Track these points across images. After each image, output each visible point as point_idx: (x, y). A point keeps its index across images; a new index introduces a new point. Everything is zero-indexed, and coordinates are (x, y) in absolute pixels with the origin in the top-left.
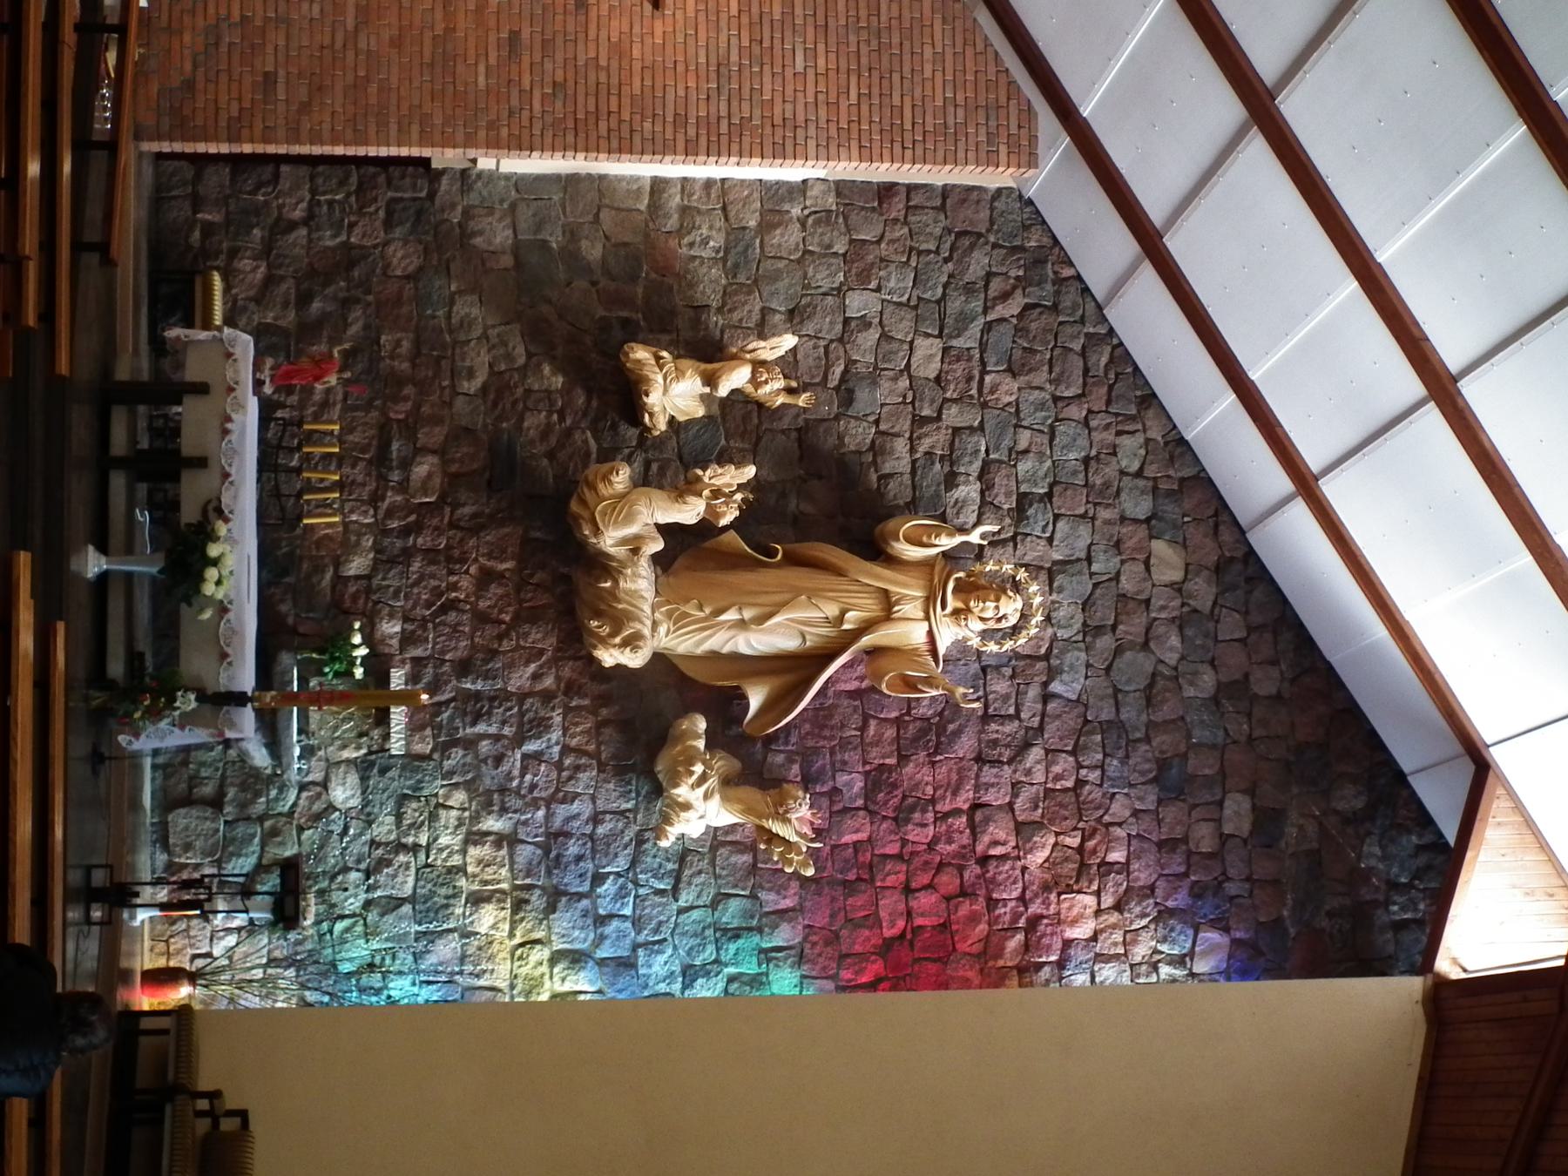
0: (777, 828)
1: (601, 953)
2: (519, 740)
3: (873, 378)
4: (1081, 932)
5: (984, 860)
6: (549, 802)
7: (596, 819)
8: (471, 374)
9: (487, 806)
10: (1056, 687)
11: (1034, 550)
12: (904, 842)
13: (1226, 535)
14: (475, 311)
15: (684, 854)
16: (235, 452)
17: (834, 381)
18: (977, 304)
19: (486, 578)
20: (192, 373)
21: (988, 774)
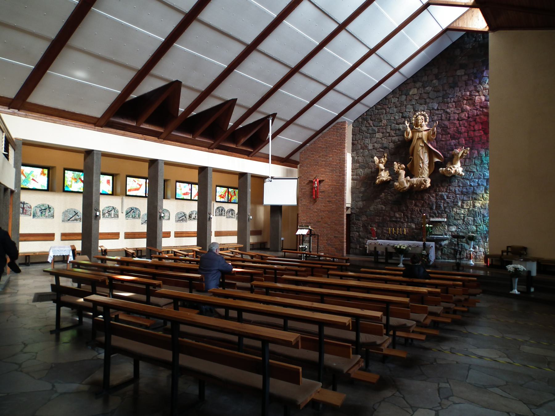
0: (460, 155)
1: (485, 184)
2: (444, 199)
3: (382, 144)
4: (483, 98)
5: (468, 117)
6: (456, 194)
7: (459, 186)
8: (382, 208)
9: (456, 205)
10: (436, 108)
11: (411, 114)
12: (465, 132)
13: (409, 81)
14: (372, 207)
15: (466, 171)
16: (385, 243)
17: (383, 150)
18: (370, 128)
19: (416, 205)
20: (373, 249)
21: (452, 118)
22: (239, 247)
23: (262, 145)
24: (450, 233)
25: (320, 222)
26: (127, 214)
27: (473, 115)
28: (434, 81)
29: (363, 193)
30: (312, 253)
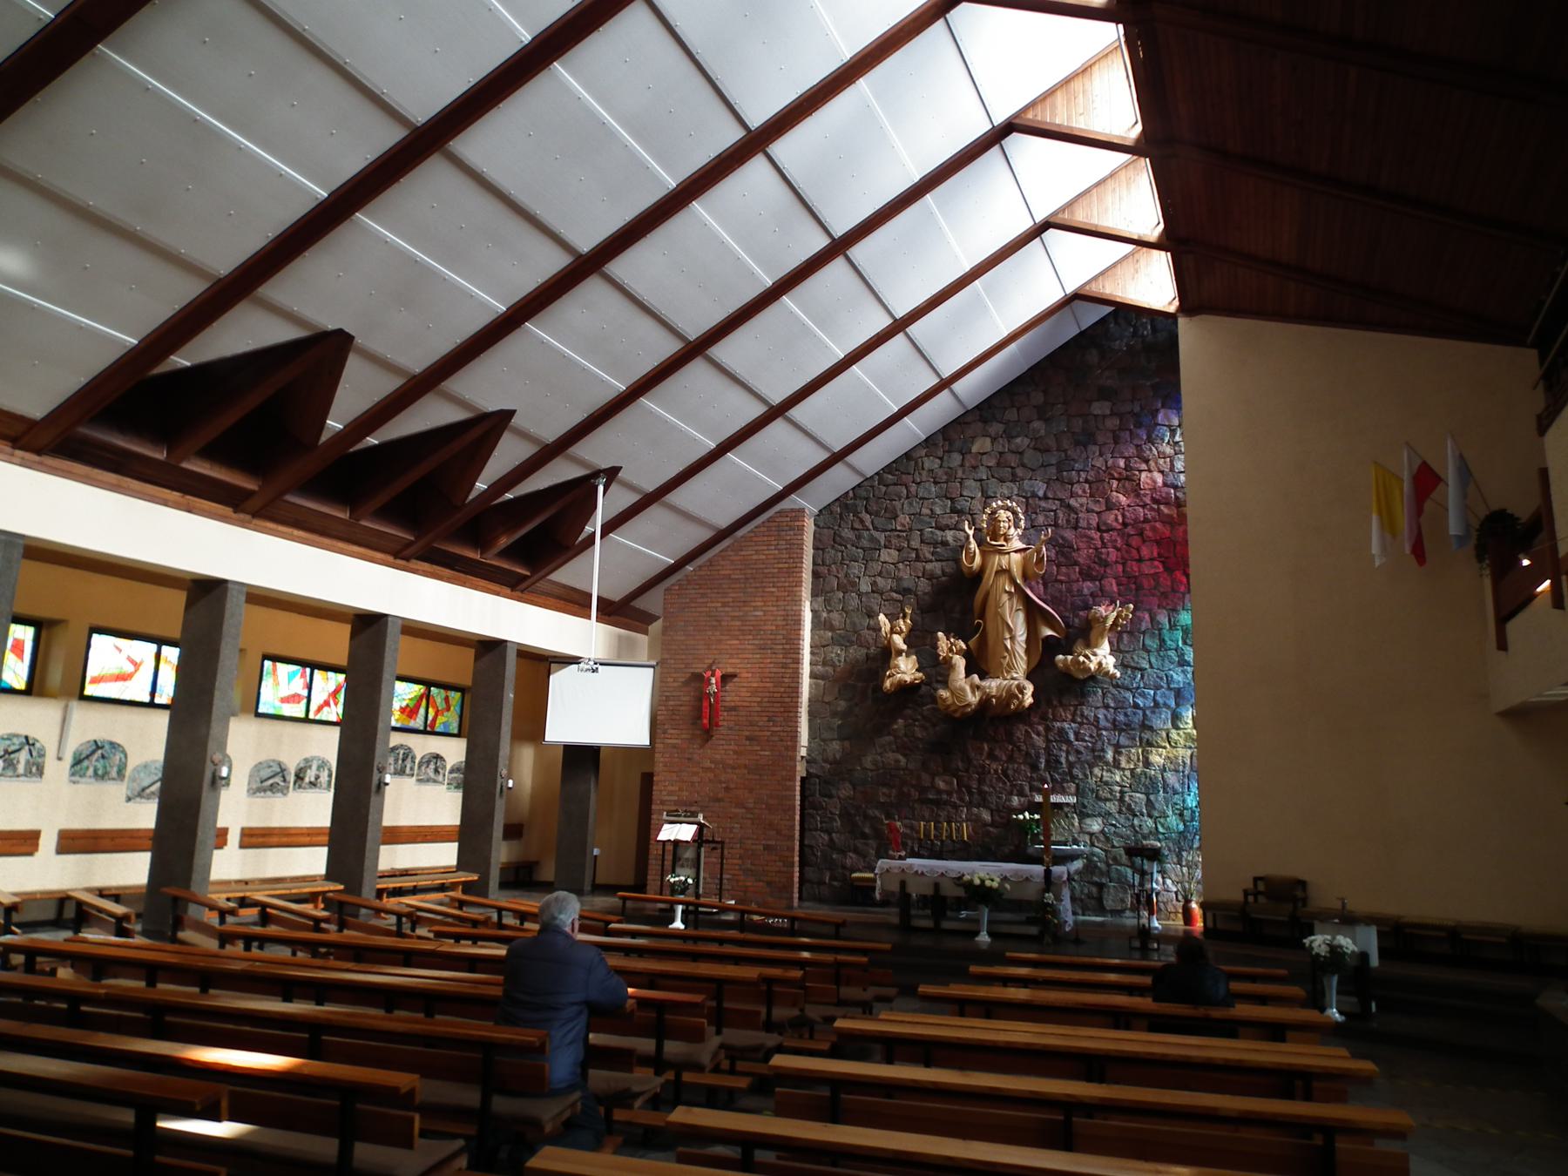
1: (1173, 704)
2: (1069, 742)
3: (899, 580)
4: (1159, 479)
5: (1125, 524)
6: (1098, 728)
7: (1107, 707)
8: (897, 761)
9: (1101, 758)
10: (1041, 493)
13: (969, 419)
14: (869, 759)
15: (1121, 665)
16: (932, 870)
17: (900, 597)
18: (865, 534)
19: (992, 756)
20: (895, 887)
21: (1083, 523)
22: (464, 883)
23: (560, 561)
24: (1087, 838)
25: (718, 800)
26: (77, 762)
27: (1136, 521)
28: (1036, 424)
29: (845, 715)
30: (702, 900)
